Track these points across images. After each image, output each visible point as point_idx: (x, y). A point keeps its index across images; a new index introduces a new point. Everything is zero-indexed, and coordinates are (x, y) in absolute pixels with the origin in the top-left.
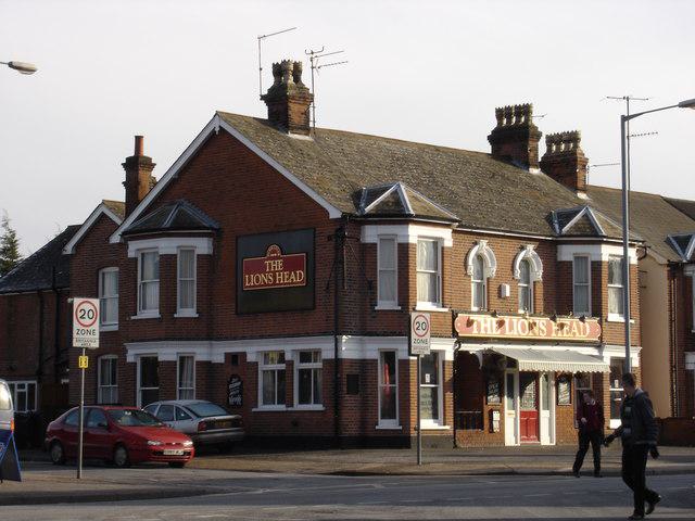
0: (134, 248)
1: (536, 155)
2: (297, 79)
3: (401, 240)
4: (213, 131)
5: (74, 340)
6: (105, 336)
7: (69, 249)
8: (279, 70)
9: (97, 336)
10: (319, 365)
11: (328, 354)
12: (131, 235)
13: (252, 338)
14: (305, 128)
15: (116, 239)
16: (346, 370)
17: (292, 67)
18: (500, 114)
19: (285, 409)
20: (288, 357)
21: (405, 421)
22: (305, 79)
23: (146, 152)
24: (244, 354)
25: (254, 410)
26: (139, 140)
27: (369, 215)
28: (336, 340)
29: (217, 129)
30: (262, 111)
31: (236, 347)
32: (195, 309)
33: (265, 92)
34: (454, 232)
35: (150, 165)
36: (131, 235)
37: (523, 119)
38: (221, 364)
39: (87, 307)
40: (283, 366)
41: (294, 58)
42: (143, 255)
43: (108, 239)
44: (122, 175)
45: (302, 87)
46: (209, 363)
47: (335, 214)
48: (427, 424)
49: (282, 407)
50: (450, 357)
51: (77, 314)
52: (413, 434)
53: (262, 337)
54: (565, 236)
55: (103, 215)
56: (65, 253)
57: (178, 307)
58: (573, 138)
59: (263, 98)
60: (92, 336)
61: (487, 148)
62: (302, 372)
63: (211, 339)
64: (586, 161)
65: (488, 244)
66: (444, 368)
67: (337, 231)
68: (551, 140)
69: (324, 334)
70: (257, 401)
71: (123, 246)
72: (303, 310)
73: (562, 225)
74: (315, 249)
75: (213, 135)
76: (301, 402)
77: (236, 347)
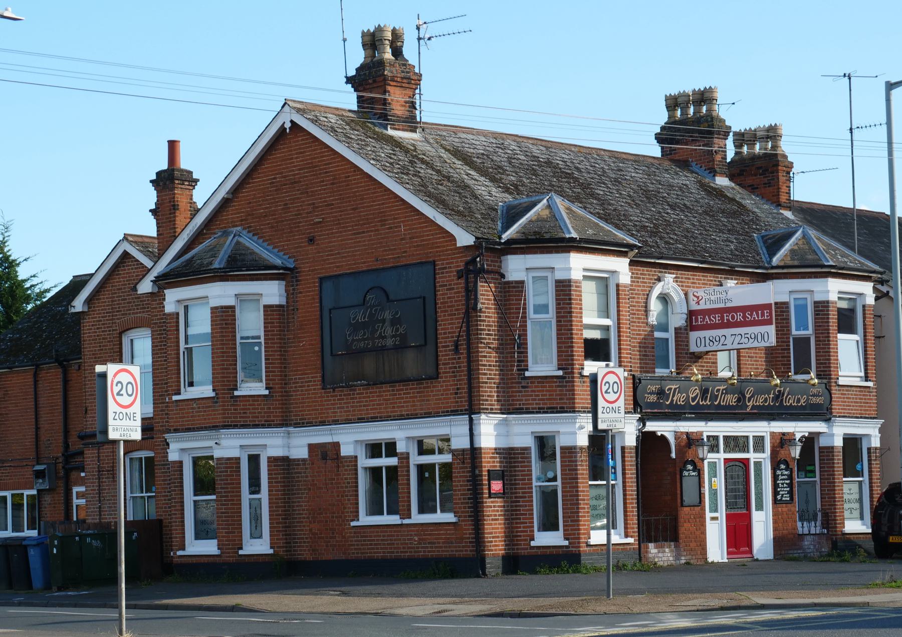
0: (173, 298)
1: (725, 158)
2: (397, 52)
3: (560, 276)
4: (282, 129)
5: (110, 429)
6: (147, 427)
7: (78, 304)
8: (372, 41)
9: (139, 423)
10: (447, 458)
11: (461, 442)
12: (167, 280)
13: (348, 421)
14: (411, 122)
15: (146, 287)
16: (489, 463)
17: (389, 36)
18: (673, 103)
19: (399, 522)
20: (401, 448)
21: (573, 533)
22: (409, 52)
23: (185, 163)
24: (336, 446)
25: (353, 524)
26: (173, 145)
27: (510, 242)
28: (471, 421)
29: (288, 125)
30: (348, 100)
31: (322, 436)
32: (264, 384)
33: (352, 72)
34: (632, 263)
35: (190, 181)
36: (167, 280)
37: (704, 109)
38: (304, 460)
39: (124, 378)
40: (393, 461)
41: (389, 23)
42: (186, 308)
43: (135, 289)
44: (151, 197)
45: (405, 63)
46: (285, 460)
47: (464, 239)
48: (598, 537)
49: (395, 519)
50: (631, 441)
51: (112, 389)
52: (583, 548)
53: (361, 420)
54: (777, 267)
55: (126, 255)
56: (73, 310)
57: (240, 375)
58: (772, 134)
59: (349, 80)
60: (617, 415)
61: (655, 151)
62: (421, 468)
63: (287, 425)
64: (790, 166)
65: (676, 280)
66: (623, 457)
67: (467, 264)
68: (742, 138)
69: (455, 413)
70: (409, 510)
71: (157, 296)
72: (419, 380)
73: (772, 253)
74: (435, 291)
75: (281, 133)
76: (422, 511)
77: (322, 436)
